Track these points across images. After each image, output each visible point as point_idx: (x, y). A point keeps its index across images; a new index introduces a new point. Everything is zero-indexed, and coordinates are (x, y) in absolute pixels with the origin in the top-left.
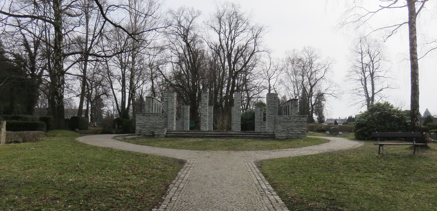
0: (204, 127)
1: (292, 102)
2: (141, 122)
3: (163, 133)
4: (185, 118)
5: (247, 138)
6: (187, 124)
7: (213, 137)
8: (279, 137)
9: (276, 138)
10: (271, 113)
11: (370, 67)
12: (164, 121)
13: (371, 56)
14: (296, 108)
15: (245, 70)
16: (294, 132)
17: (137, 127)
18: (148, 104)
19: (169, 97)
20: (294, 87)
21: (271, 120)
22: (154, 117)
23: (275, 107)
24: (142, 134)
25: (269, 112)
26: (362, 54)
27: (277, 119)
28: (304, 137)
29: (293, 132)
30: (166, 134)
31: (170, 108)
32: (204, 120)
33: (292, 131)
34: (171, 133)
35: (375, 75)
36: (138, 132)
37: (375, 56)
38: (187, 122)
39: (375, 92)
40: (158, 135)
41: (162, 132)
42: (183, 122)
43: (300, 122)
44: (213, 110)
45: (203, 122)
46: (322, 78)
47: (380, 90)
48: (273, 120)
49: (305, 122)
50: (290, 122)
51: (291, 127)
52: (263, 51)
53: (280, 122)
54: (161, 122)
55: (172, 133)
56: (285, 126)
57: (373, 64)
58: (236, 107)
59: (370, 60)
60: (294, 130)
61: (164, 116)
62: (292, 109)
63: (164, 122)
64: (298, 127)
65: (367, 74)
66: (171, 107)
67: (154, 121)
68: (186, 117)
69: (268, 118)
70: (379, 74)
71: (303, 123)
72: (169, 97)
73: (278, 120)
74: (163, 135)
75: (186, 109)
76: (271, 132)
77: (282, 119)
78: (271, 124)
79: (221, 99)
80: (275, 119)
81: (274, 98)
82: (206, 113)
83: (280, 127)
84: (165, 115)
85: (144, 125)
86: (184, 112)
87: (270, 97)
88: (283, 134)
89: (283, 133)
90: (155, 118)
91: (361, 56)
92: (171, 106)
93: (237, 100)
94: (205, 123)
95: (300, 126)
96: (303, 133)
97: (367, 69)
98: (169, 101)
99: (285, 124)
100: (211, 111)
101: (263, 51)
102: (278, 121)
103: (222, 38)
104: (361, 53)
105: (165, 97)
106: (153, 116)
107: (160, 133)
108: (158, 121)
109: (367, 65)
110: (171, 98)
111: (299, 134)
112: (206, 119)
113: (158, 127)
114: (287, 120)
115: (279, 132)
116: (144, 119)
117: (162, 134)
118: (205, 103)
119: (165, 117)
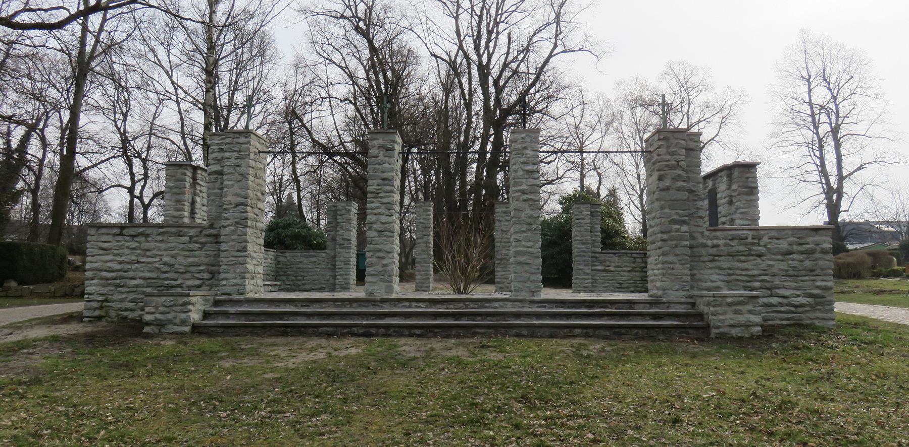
0: (382, 280)
1: (730, 176)
2: (109, 264)
3: (183, 316)
4: (342, 242)
5: (578, 331)
6: (347, 263)
7: (418, 332)
8: (732, 326)
9: (714, 331)
10: (675, 217)
11: (829, 112)
12: (208, 256)
13: (832, 86)
14: (749, 198)
15: (523, 108)
16: (780, 300)
17: (91, 285)
18: (175, 190)
19: (227, 154)
20: (637, 168)
21: (676, 246)
22: (165, 238)
23: (691, 191)
24: (113, 313)
25: (667, 210)
26: (808, 80)
27: (702, 241)
28: (824, 319)
29: (774, 300)
30: (206, 315)
31: (230, 198)
32: (380, 251)
33: (771, 296)
34: (226, 314)
35: (843, 131)
36: (95, 305)
37: (841, 85)
38: (347, 255)
39: (845, 173)
40: (161, 324)
41: (178, 308)
42: (334, 257)
43: (802, 253)
44: (432, 217)
45: (374, 260)
46: (713, 139)
47: (859, 169)
48: (685, 246)
49: (824, 252)
50: (760, 256)
51: (766, 278)
52: (580, 50)
53: (714, 258)
54: (190, 260)
55: (232, 310)
56: (739, 272)
57: (837, 106)
58: (519, 191)
59: (830, 95)
60: (778, 291)
61: (209, 236)
62: (731, 203)
63: (206, 260)
64: (793, 275)
65: (824, 128)
66: (237, 195)
67: (165, 259)
68: (344, 239)
69: (665, 236)
70: (854, 129)
71: (816, 260)
72: (227, 154)
73: (705, 246)
74: (184, 322)
75: (344, 211)
76: (683, 300)
77: (721, 242)
78: (678, 266)
79: (463, 193)
80: (692, 242)
81: (684, 152)
82: (390, 219)
83: (714, 277)
84: (213, 232)
85: (121, 273)
86: (336, 223)
87: (668, 147)
88: (750, 312)
89: (750, 307)
90: (169, 245)
91: (807, 86)
92: (238, 191)
93: (523, 159)
94: (385, 265)
95: (803, 273)
96: (817, 304)
97: (824, 118)
98: (226, 170)
99: (739, 265)
100: (425, 219)
101: (580, 50)
102: (703, 251)
103: (465, 27)
104: (807, 77)
105: (215, 155)
106: (160, 238)
107: (170, 316)
108: (180, 259)
109: (822, 107)
110: (237, 158)
111: (802, 306)
112: (387, 247)
113: (179, 282)
114: (746, 244)
115: (730, 305)
116: (121, 251)
117: (177, 321)
118: (385, 175)
119: (209, 239)
